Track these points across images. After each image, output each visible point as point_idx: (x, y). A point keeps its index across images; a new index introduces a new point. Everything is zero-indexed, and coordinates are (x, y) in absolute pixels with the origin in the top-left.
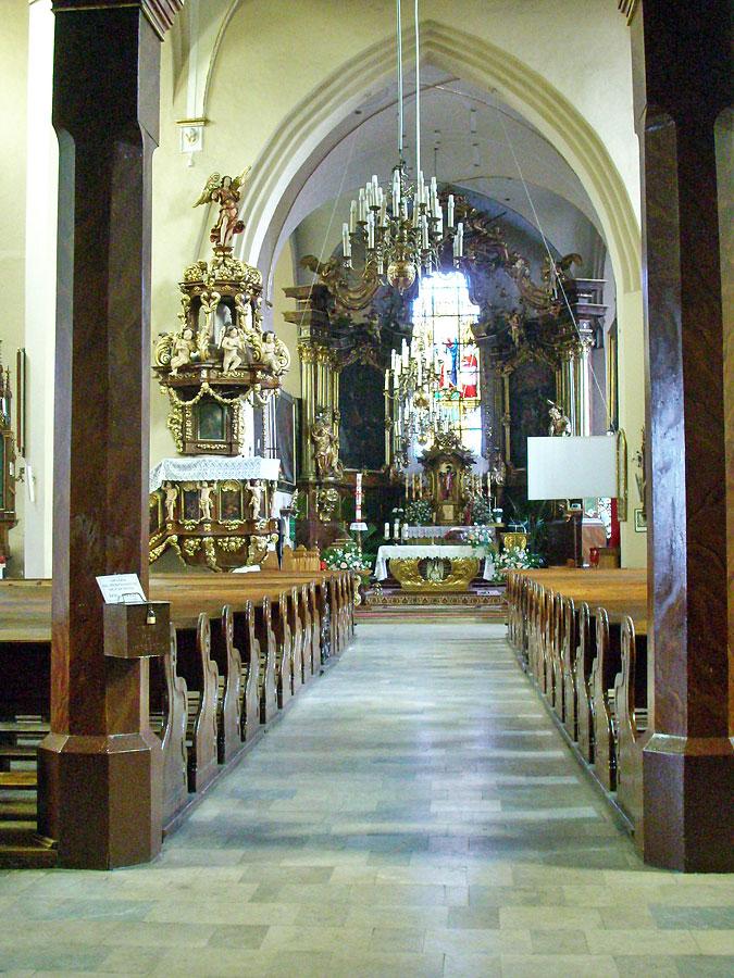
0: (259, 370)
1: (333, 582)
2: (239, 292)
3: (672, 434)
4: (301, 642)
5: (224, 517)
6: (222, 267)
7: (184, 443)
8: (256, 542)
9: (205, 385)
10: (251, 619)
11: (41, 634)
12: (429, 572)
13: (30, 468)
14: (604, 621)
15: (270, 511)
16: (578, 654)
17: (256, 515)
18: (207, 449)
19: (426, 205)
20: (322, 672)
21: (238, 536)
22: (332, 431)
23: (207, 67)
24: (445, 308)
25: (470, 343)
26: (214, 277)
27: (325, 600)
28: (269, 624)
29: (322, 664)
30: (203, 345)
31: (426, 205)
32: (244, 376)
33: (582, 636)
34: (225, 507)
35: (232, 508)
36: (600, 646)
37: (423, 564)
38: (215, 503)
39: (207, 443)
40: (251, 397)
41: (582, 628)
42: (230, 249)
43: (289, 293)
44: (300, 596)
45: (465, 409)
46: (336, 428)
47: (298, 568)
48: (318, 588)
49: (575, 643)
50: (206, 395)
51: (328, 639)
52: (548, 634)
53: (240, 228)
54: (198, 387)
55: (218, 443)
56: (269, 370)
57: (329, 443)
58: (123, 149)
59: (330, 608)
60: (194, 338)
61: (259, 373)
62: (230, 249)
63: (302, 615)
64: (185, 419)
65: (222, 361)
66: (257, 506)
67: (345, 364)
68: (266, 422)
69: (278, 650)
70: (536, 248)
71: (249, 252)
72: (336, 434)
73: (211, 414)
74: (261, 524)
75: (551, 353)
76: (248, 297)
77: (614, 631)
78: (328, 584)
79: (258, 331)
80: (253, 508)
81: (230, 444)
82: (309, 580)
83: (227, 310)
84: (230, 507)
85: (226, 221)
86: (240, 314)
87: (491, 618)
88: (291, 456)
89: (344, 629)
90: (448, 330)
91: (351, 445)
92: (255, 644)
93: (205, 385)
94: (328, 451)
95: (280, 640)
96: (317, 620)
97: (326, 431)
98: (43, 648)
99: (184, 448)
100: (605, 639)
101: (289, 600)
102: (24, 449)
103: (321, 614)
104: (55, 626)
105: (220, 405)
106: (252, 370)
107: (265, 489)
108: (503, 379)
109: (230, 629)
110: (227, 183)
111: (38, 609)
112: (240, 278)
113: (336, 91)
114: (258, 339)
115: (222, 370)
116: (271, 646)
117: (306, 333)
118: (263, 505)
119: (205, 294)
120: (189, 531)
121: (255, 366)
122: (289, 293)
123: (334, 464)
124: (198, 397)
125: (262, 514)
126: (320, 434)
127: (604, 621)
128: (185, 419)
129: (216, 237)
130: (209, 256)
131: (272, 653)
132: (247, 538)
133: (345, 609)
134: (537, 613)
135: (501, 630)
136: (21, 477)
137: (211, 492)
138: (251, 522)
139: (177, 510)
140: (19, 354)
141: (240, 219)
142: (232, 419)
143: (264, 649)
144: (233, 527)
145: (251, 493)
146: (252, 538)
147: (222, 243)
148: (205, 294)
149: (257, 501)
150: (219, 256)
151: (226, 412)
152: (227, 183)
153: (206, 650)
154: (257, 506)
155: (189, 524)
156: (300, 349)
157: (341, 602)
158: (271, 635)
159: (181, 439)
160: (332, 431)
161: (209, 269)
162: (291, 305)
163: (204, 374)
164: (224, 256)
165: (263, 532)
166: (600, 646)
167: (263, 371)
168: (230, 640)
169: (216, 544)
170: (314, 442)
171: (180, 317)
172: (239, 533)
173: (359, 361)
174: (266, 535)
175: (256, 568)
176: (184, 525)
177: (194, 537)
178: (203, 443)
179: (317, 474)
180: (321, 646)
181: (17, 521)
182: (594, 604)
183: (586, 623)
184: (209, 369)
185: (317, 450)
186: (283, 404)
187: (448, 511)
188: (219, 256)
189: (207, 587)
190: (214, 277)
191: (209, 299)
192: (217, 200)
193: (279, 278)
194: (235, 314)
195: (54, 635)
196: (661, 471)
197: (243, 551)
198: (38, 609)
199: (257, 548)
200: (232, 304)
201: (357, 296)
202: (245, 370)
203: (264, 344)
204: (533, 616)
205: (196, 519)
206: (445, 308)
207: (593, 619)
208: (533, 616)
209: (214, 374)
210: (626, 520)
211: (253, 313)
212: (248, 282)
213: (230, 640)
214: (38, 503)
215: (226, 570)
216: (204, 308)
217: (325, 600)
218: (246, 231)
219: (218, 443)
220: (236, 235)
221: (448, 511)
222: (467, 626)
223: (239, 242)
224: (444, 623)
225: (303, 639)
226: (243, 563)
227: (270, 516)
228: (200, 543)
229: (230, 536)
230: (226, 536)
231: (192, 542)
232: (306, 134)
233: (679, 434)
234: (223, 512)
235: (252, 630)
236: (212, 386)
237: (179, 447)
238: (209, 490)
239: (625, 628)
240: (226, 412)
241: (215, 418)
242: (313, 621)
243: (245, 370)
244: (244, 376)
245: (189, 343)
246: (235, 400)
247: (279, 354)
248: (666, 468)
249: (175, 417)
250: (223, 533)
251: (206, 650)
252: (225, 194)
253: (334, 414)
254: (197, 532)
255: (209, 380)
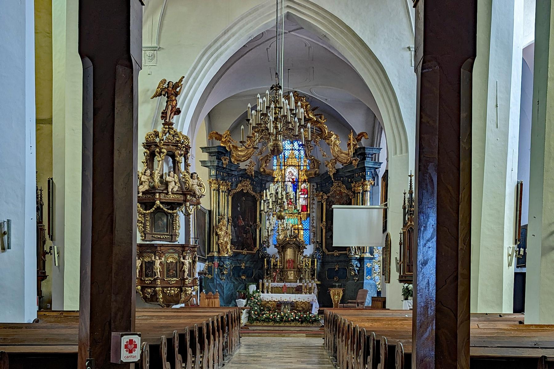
0: (188, 194)
1: (230, 315)
2: (177, 149)
3: (429, 244)
4: (213, 350)
5: (167, 277)
6: (168, 134)
7: (145, 234)
8: (186, 290)
9: (158, 202)
10: (188, 338)
11: (75, 349)
12: (282, 308)
13: (55, 247)
14: (385, 344)
15: (193, 273)
16: (369, 360)
17: (186, 276)
18: (158, 238)
19: (293, 110)
20: (224, 365)
21: (176, 287)
22: (227, 229)
23: (158, 17)
24: (291, 165)
25: (305, 181)
26: (163, 140)
27: (225, 325)
28: (197, 339)
29: (224, 360)
30: (157, 179)
31: (293, 110)
32: (181, 198)
33: (371, 351)
34: (168, 271)
35: (172, 272)
36: (382, 357)
37: (279, 304)
38: (163, 268)
39: (158, 234)
40: (183, 209)
41: (371, 346)
42: (172, 124)
43: (204, 149)
44: (213, 322)
45: (301, 218)
46: (229, 227)
47: (208, 305)
48: (222, 317)
49: (367, 353)
50: (159, 208)
51: (227, 346)
52: (350, 346)
53: (178, 112)
54: (154, 203)
55: (164, 235)
56: (194, 195)
57: (225, 235)
58: (121, 70)
59: (228, 329)
60: (152, 175)
61: (189, 196)
62: (172, 124)
63: (214, 334)
64: (146, 221)
65: (167, 188)
66: (187, 270)
67: (234, 191)
68: (191, 223)
69: (201, 353)
70: (344, 128)
71: (182, 125)
72: (229, 231)
73: (160, 218)
74: (188, 281)
75: (349, 188)
76: (182, 152)
77: (391, 349)
78: (227, 315)
79: (187, 172)
80: (184, 271)
81: (172, 235)
82: (217, 314)
83: (170, 160)
84: (171, 271)
85: (170, 107)
86: (178, 162)
87: (315, 335)
88: (204, 242)
89: (235, 339)
90: (292, 172)
91: (237, 237)
92: (189, 351)
93: (158, 202)
94: (225, 239)
95: (202, 349)
96: (221, 336)
97: (224, 228)
98: (74, 356)
99: (145, 237)
100: (385, 354)
101: (208, 325)
102: (52, 236)
103: (223, 333)
104: (81, 345)
105: (167, 214)
106: (185, 195)
107: (191, 261)
108: (322, 204)
109: (177, 344)
110: (171, 85)
111: (69, 331)
112: (178, 141)
113: (233, 35)
114: (188, 176)
115: (167, 194)
116: (198, 351)
117: (213, 172)
118: (190, 270)
119: (158, 150)
120: (147, 284)
121: (187, 193)
122: (204, 149)
123: (229, 247)
124: (153, 209)
125: (189, 275)
126: (221, 230)
127: (385, 344)
128: (146, 221)
129: (164, 117)
130: (160, 128)
131: (198, 355)
132: (181, 288)
133: (236, 331)
134: (343, 335)
135: (320, 341)
136: (50, 252)
137: (161, 262)
138: (183, 280)
139: (141, 271)
140: (49, 181)
141: (177, 107)
142: (173, 221)
143: (194, 353)
144: (173, 282)
145: (183, 263)
146: (183, 289)
147: (167, 120)
148: (158, 150)
149: (186, 268)
150: (166, 128)
151: (169, 218)
152: (171, 85)
153: (164, 356)
154: (187, 270)
155: (148, 280)
156: (210, 182)
157: (234, 325)
158: (198, 346)
159: (144, 232)
160: (227, 229)
161: (160, 135)
162: (205, 157)
163: (157, 196)
164: (169, 128)
165: (189, 285)
166: (382, 357)
167: (191, 195)
168: (177, 349)
169: (163, 292)
170: (217, 234)
171: (143, 162)
172: (177, 285)
173: (243, 189)
174: (191, 287)
175: (183, 305)
176: (145, 280)
177: (150, 287)
178: (156, 234)
179: (219, 252)
180: (223, 350)
181: (46, 276)
182: (380, 333)
183: (374, 343)
184: (160, 193)
185: (218, 239)
186: (200, 213)
187: (291, 275)
188: (166, 128)
189: (159, 317)
190: (163, 140)
191: (160, 153)
192: (164, 95)
193: (198, 141)
194: (174, 162)
195: (80, 349)
196: (422, 264)
197: (178, 295)
198: (69, 331)
199: (186, 294)
200: (173, 156)
201: (243, 154)
202: (181, 194)
203: (191, 180)
204: (340, 335)
205: (152, 277)
206: (291, 165)
207: (378, 342)
208: (340, 335)
209: (162, 196)
210: (389, 282)
211: (185, 161)
212: (182, 144)
213: (177, 349)
214: (60, 267)
215: (168, 306)
216: (157, 158)
217: (225, 325)
218: (181, 114)
219: (164, 235)
220: (175, 116)
221: (291, 275)
222: (302, 338)
223: (178, 121)
224: (288, 336)
225: (214, 347)
226: (177, 303)
227: (193, 276)
228: (154, 291)
229: (171, 287)
230: (168, 287)
231: (149, 290)
232: (217, 58)
233: (433, 244)
234: (167, 274)
235: (188, 343)
236: (161, 203)
237: (142, 236)
238: (159, 261)
239: (382, 342)
240: (169, 218)
241: (162, 221)
242: (219, 337)
243: (181, 194)
244: (181, 198)
245: (149, 178)
246: (175, 211)
247: (200, 185)
248: (425, 263)
249: (140, 219)
250: (168, 285)
251: (164, 356)
252: (170, 91)
253: (228, 219)
254: (153, 285)
255: (160, 199)
